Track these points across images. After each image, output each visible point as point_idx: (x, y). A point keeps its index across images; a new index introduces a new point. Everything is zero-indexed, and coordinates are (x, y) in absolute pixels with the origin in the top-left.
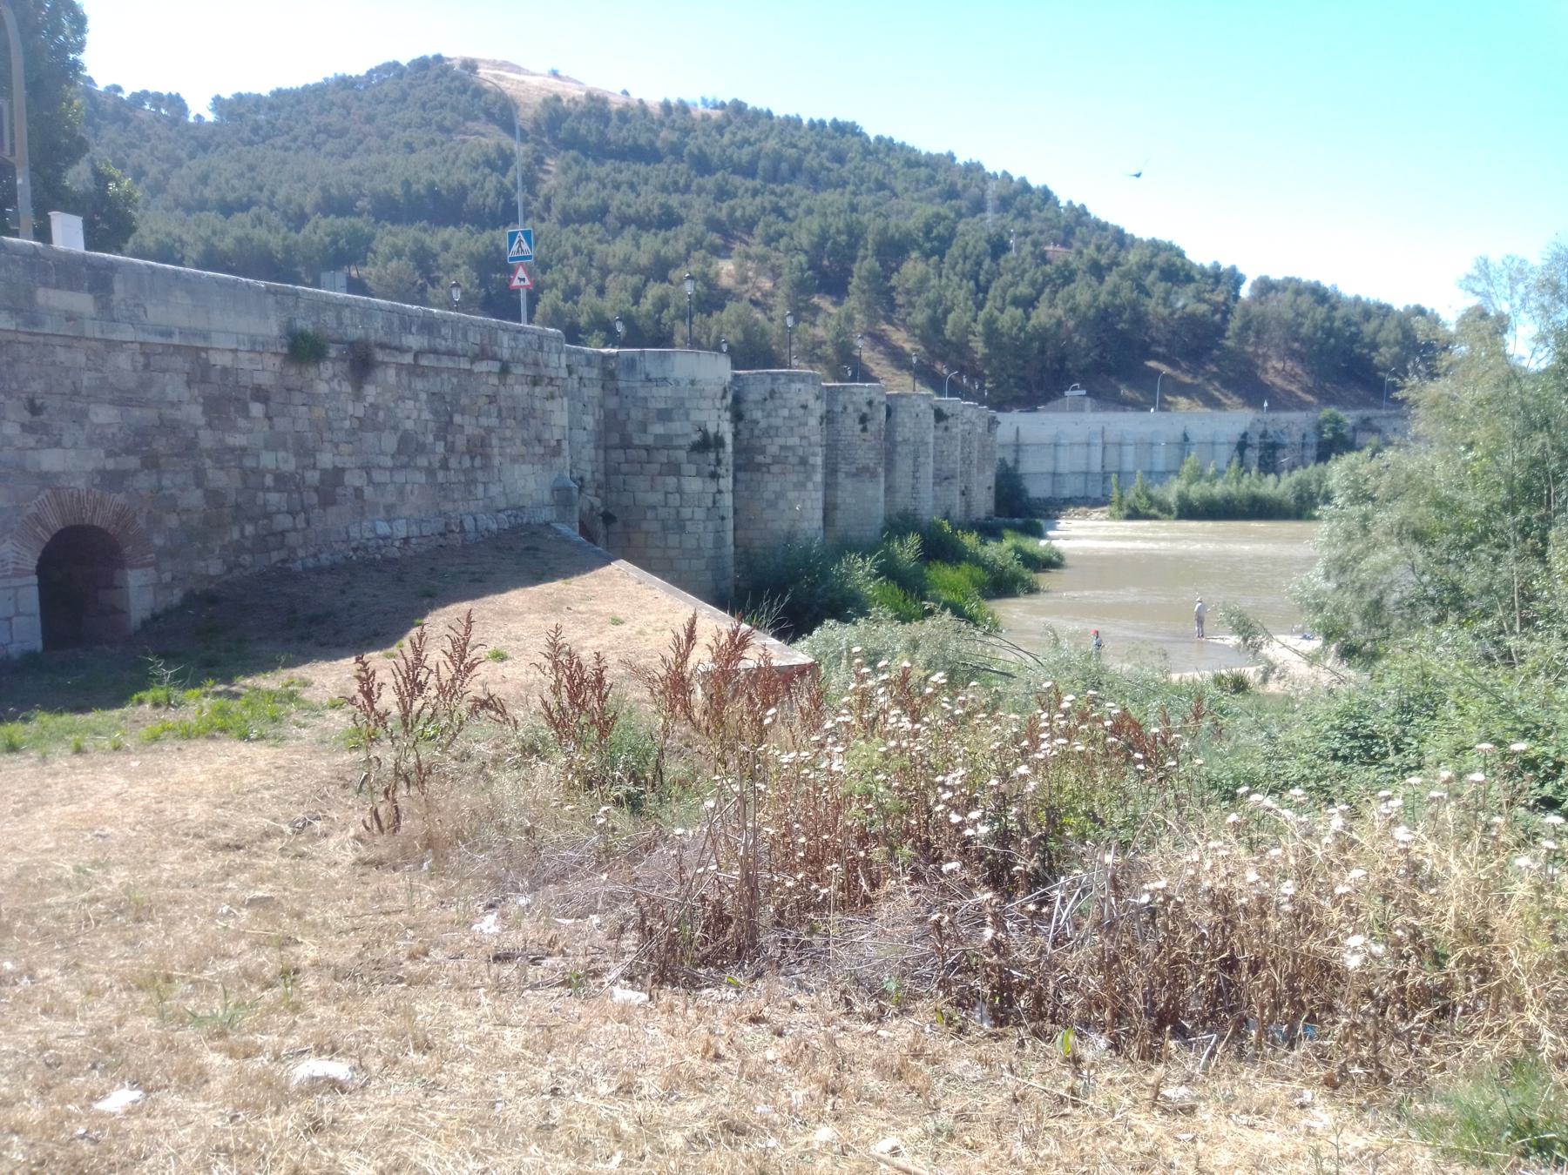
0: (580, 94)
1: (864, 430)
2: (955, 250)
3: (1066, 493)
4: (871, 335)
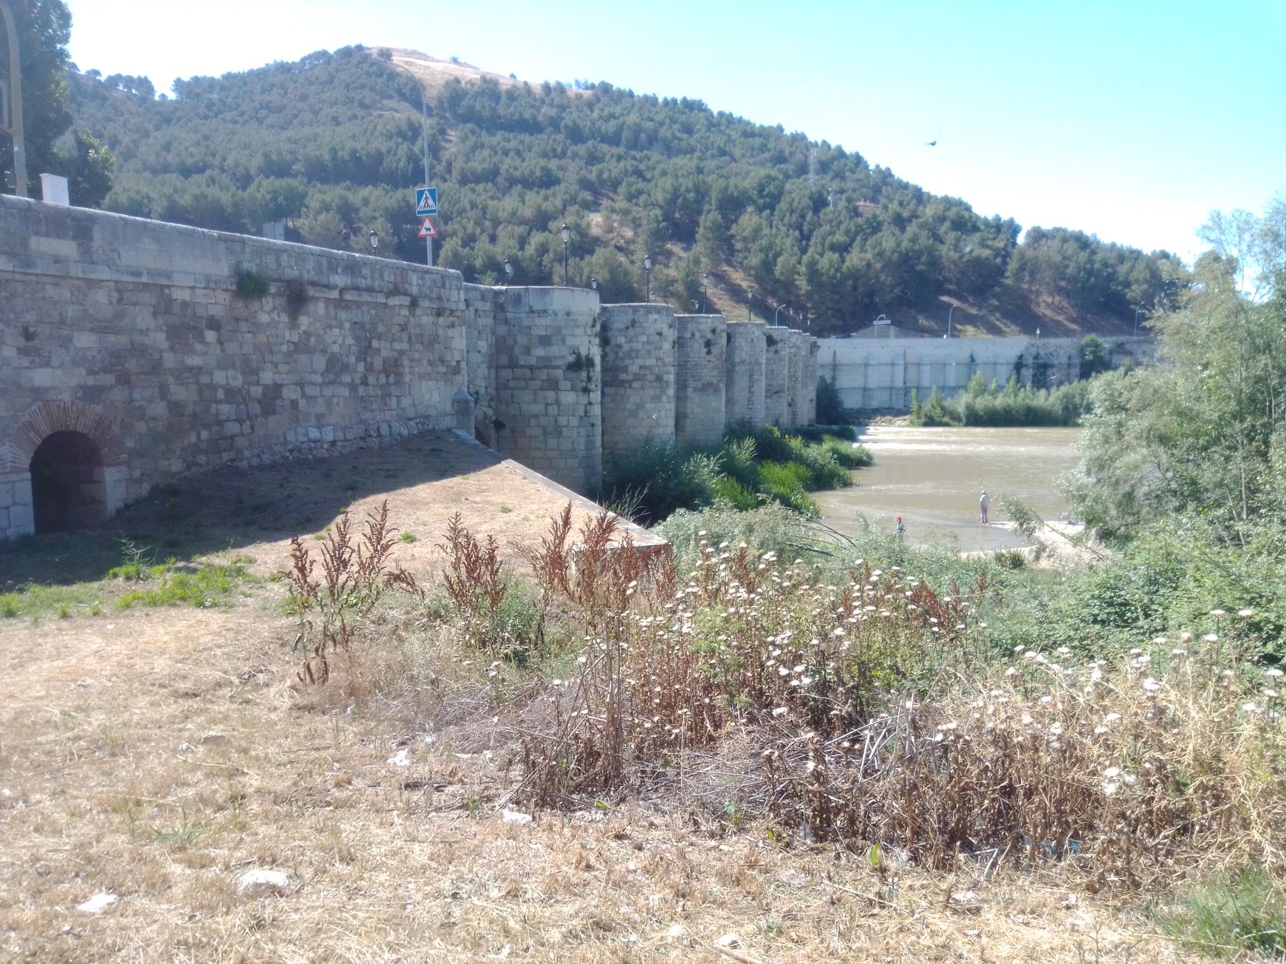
0: (476, 77)
1: (709, 353)
2: (783, 205)
3: (875, 404)
4: (714, 275)
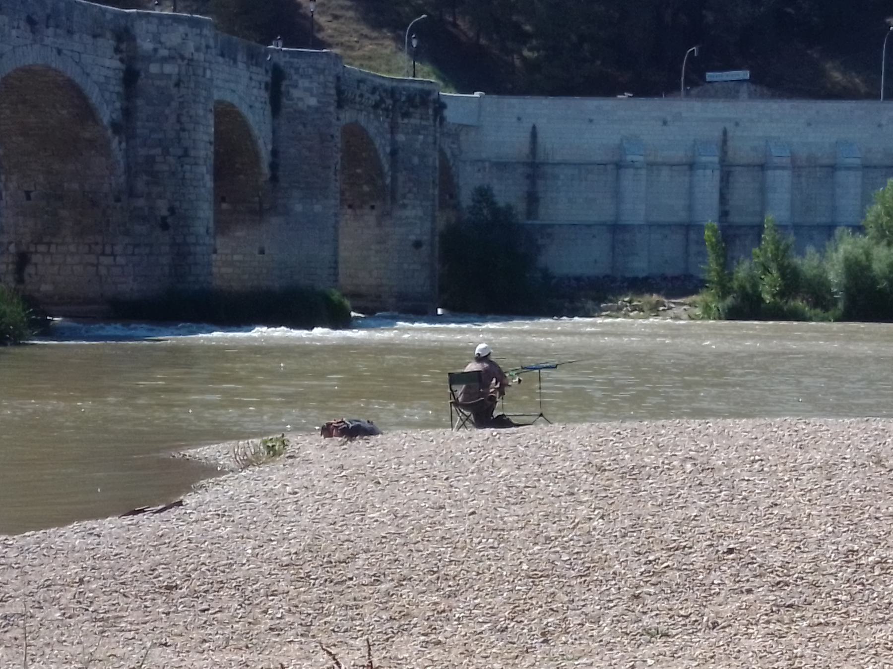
3: (640, 266)
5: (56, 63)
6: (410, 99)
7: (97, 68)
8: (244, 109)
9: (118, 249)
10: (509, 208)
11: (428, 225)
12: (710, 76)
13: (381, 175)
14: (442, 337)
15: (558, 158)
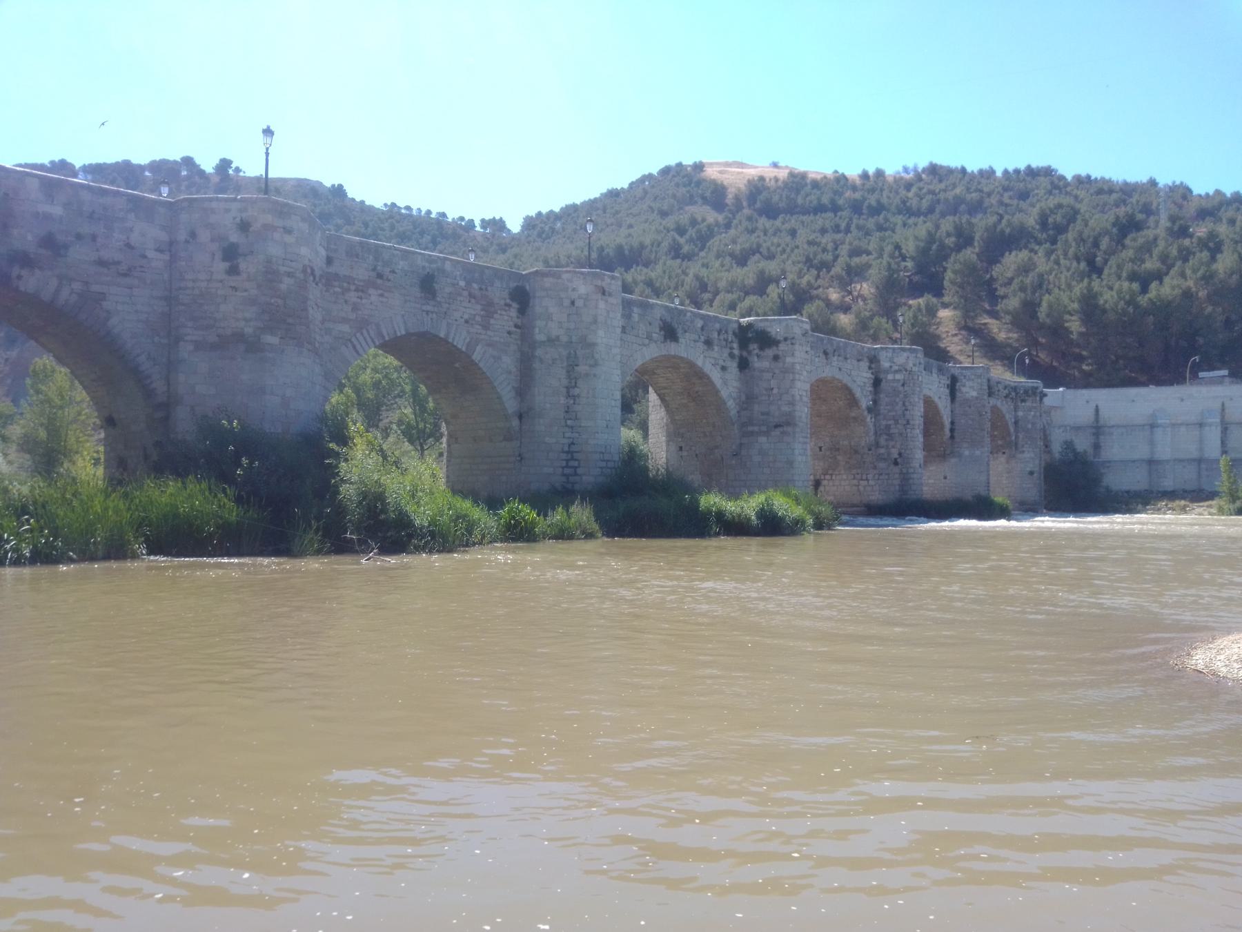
0: (783, 174)
1: (233, 271)
2: (1071, 235)
3: (1168, 484)
4: (966, 328)
5: (838, 376)
6: (1026, 392)
7: (859, 378)
8: (936, 399)
9: (870, 477)
10: (1085, 452)
11: (1037, 462)
12: (1201, 374)
13: (1009, 434)
14: (1096, 526)
15: (1112, 423)
